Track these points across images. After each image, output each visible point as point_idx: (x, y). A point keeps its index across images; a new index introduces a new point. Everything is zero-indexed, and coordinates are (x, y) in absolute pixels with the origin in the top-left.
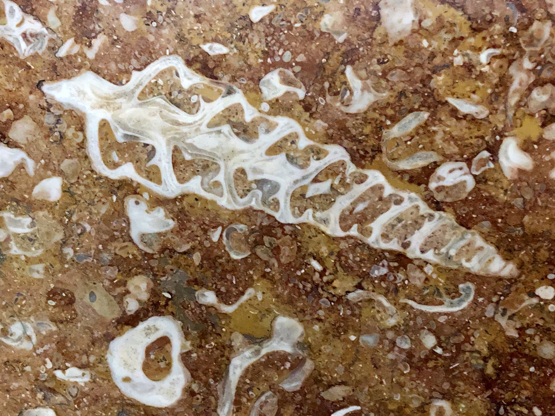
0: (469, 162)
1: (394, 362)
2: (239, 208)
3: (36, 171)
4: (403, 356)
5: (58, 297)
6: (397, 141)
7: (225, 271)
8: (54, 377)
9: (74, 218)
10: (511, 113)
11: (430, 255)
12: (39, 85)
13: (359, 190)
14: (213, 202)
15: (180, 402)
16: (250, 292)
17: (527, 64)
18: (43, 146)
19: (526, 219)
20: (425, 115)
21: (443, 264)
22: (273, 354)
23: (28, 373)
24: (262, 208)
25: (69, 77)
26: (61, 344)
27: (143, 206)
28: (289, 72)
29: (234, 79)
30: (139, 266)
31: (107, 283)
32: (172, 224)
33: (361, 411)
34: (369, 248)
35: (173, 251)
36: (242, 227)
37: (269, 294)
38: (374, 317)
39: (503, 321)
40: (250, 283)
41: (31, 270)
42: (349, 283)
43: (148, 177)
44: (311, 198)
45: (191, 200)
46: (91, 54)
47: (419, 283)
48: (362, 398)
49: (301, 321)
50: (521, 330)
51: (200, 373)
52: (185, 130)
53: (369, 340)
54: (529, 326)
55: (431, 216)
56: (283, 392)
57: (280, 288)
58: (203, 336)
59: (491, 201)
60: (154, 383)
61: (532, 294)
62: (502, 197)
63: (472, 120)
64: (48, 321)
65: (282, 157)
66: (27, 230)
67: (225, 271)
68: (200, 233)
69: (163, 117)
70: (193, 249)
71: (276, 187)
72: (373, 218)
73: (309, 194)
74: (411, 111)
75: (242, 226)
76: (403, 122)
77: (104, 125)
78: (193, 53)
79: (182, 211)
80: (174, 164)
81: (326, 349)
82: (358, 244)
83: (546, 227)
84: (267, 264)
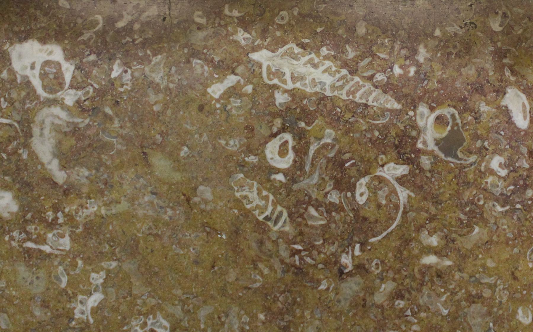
0: (385, 72)
1: (366, 143)
2: (313, 92)
3: (244, 83)
4: (369, 140)
5: (248, 129)
6: (363, 67)
7: (308, 114)
8: (245, 160)
9: (256, 99)
10: (395, 57)
11: (375, 104)
12: (248, 54)
13: (352, 83)
14: (304, 90)
15: (291, 166)
16: (317, 121)
17: (399, 43)
18: (247, 74)
19: (403, 90)
20: (371, 59)
21: (379, 106)
22: (325, 143)
23: (234, 160)
24: (320, 91)
25: (257, 51)
26: (248, 147)
27: (280, 93)
28: (329, 47)
29: (312, 50)
30: (278, 115)
31: (266, 122)
32: (290, 99)
33: (355, 162)
34: (356, 103)
35: (290, 108)
36: (314, 98)
37: (323, 121)
38: (358, 127)
39: (399, 124)
40: (316, 118)
41: (239, 119)
42: (350, 115)
43: (282, 83)
44: (337, 87)
45: (297, 90)
46: (266, 44)
47: (372, 113)
48: (356, 158)
49: (334, 130)
50: (405, 127)
51: (299, 154)
52: (295, 66)
53: (357, 135)
54: (407, 125)
55: (375, 91)
56: (328, 158)
57: (484, 108)
58: (300, 139)
59: (392, 84)
60: (282, 159)
61: (407, 114)
62: (395, 83)
63: (385, 59)
64: (244, 138)
65: (327, 74)
66: (239, 104)
67: (308, 114)
68: (299, 101)
69: (288, 63)
70: (297, 107)
71: (325, 84)
72: (357, 92)
73: (336, 86)
74: (367, 57)
75: (314, 98)
76: (365, 61)
77: (269, 67)
78: (299, 42)
79: (293, 94)
80: (291, 78)
81: (343, 140)
82: (352, 102)
83: (409, 92)
84: (322, 111)
